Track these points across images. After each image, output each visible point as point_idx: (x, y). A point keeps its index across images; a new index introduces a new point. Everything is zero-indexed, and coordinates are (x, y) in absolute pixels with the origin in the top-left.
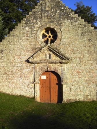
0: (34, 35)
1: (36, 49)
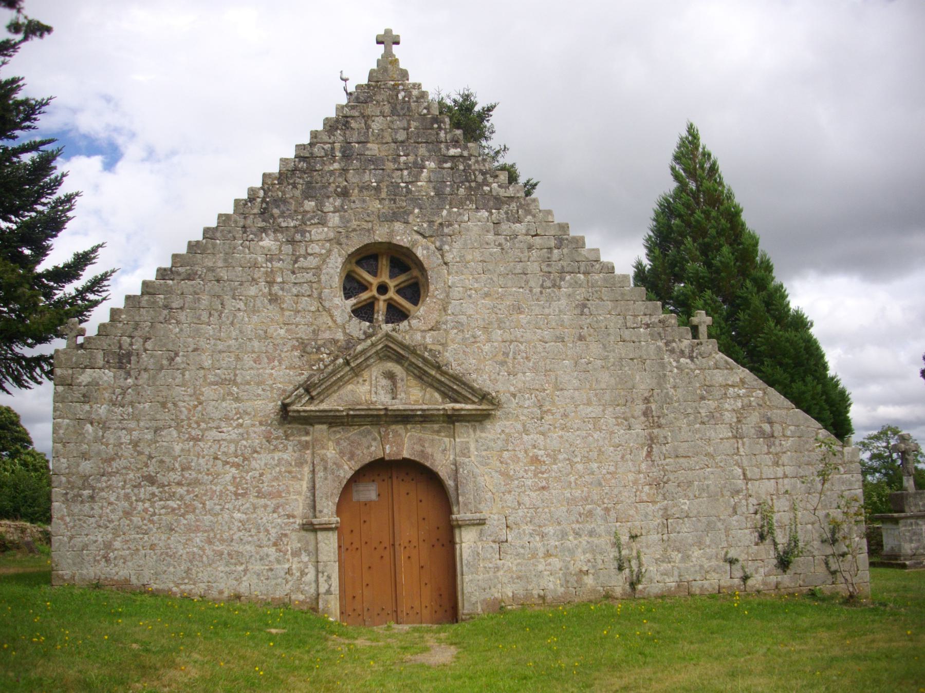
0: (309, 276)
1: (318, 349)
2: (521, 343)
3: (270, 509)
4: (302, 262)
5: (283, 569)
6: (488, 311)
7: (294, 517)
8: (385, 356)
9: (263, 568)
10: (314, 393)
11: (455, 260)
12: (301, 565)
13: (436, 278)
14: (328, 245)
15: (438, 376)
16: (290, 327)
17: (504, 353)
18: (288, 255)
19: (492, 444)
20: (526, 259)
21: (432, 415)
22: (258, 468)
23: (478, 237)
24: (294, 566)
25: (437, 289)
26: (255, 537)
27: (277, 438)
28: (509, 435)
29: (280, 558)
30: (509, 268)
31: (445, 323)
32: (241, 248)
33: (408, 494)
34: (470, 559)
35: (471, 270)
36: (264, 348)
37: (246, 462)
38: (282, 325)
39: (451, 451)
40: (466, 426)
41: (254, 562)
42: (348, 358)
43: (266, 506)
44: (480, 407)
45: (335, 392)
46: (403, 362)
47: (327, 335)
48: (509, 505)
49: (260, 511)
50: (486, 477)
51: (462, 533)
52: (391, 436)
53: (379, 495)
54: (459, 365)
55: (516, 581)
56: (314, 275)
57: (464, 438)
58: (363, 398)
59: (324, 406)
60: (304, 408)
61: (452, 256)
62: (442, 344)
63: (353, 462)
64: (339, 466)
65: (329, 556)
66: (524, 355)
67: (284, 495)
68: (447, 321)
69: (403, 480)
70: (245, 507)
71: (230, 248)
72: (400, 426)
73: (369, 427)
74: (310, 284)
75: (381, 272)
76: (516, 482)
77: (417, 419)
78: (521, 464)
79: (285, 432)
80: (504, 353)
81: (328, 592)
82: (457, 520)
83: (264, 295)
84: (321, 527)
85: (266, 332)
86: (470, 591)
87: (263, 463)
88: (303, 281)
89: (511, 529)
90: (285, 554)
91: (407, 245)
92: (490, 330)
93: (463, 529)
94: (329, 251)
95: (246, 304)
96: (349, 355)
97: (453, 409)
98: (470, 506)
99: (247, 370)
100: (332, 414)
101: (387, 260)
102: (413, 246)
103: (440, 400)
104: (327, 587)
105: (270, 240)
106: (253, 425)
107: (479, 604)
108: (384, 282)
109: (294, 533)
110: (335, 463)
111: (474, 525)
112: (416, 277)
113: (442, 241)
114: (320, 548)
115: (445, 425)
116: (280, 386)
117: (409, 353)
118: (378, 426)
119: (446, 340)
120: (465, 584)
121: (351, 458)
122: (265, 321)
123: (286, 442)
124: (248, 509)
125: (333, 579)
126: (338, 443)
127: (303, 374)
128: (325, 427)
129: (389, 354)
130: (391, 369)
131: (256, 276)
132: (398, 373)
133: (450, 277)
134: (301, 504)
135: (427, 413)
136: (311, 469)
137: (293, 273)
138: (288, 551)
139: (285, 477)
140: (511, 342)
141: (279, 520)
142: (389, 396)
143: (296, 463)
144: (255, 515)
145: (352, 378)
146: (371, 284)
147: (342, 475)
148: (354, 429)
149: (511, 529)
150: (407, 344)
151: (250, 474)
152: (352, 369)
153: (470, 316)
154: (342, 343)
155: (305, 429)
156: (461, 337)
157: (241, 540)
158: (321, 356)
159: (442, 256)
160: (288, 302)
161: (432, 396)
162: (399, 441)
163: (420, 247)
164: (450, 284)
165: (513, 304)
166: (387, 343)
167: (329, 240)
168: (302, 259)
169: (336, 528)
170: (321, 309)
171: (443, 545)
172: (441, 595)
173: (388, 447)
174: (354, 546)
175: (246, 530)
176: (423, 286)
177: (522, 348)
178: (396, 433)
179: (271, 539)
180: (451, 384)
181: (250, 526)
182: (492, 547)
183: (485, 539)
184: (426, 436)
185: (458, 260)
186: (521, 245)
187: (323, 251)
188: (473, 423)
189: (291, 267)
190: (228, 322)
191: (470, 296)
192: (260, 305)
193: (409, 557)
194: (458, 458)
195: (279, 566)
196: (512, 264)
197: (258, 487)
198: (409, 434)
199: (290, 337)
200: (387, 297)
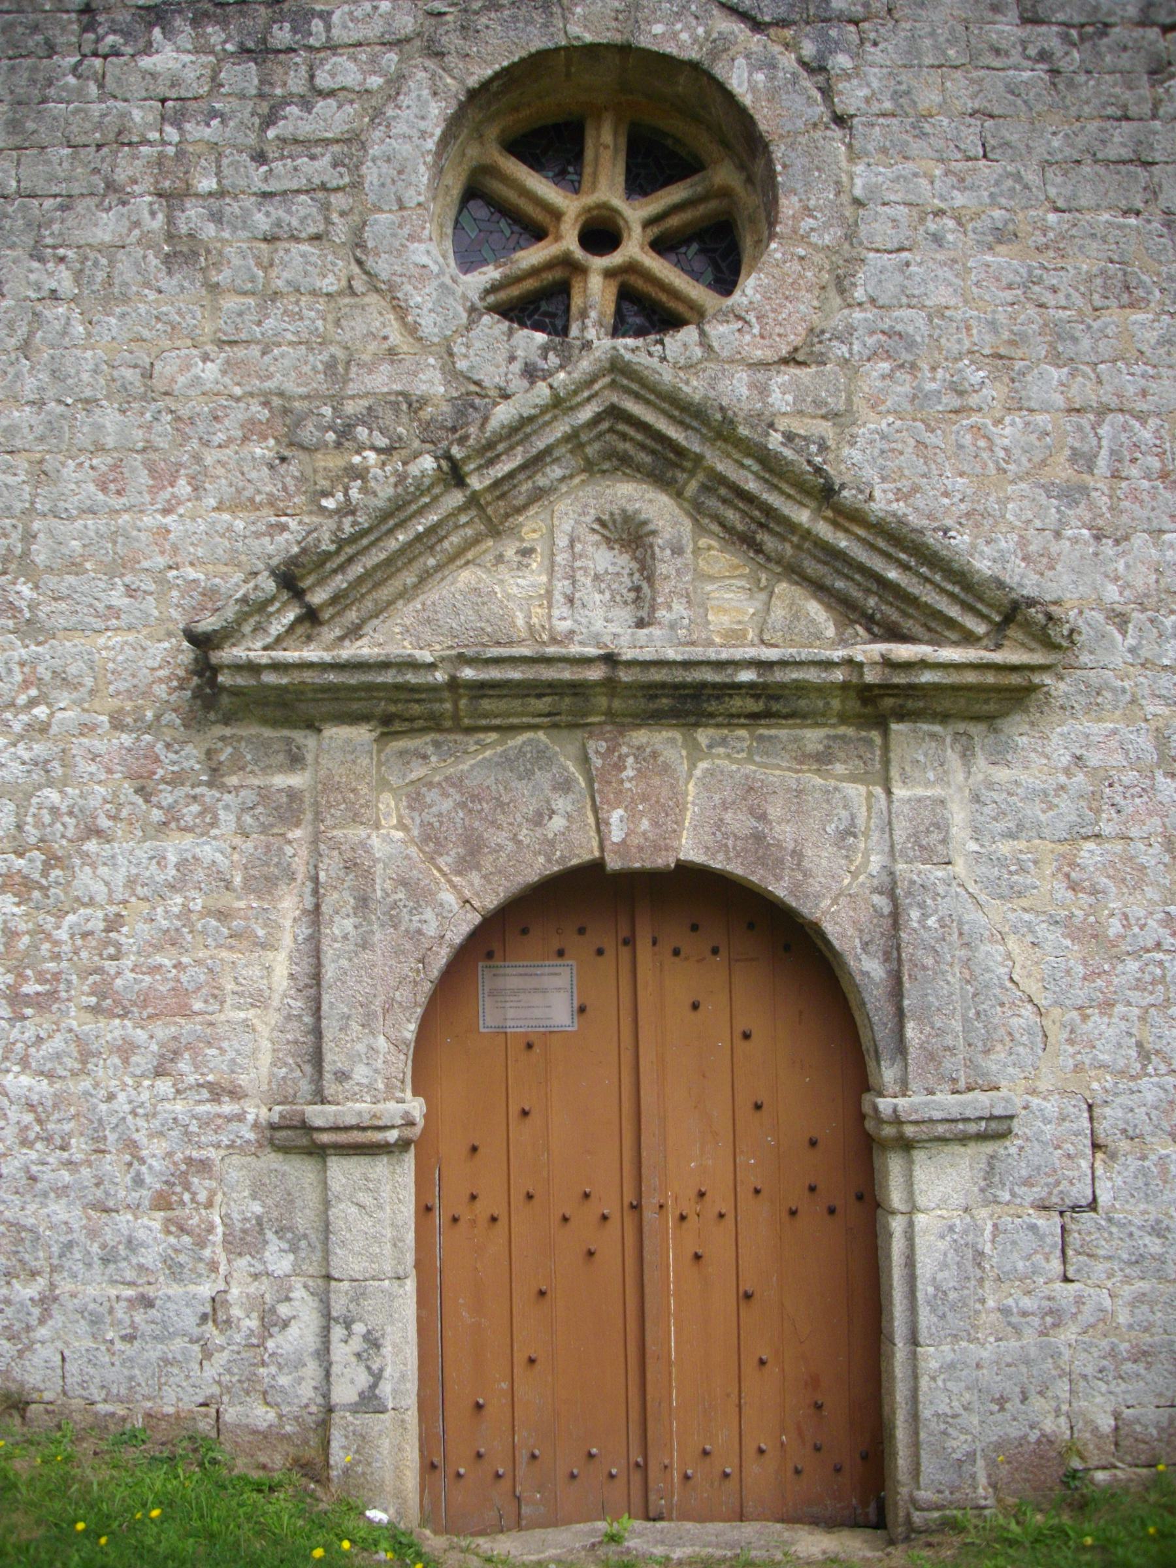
0: (319, 168)
1: (345, 433)
2: (1142, 417)
3: (142, 1062)
4: (294, 122)
5: (192, 1299)
6: (1009, 296)
7: (236, 1094)
8: (609, 454)
9: (113, 1292)
10: (317, 598)
11: (875, 107)
12: (264, 1285)
13: (807, 171)
14: (391, 57)
15: (824, 530)
16: (240, 352)
17: (1075, 455)
18: (242, 96)
19: (1035, 811)
20: (1147, 109)
21: (801, 688)
22: (101, 898)
23: (960, 28)
24: (235, 1291)
25: (808, 211)
26: (85, 1172)
27: (176, 780)
28: (1104, 777)
29: (182, 1258)
30: (1081, 141)
31: (845, 335)
32: (71, 80)
33: (695, 1006)
34: (948, 1278)
35: (941, 144)
36: (139, 434)
37: (56, 873)
38: (209, 348)
39: (875, 836)
40: (933, 736)
41: (79, 1267)
42: (456, 451)
43: (126, 1050)
44: (998, 657)
45: (405, 594)
46: (681, 476)
47: (382, 380)
48: (1105, 1057)
49: (105, 1070)
50: (1012, 943)
51: (919, 1174)
52: (630, 773)
53: (582, 1010)
54: (900, 495)
55: (1129, 1367)
56: (335, 165)
57: (928, 784)
58: (520, 622)
59: (363, 649)
60: (279, 655)
61: (864, 92)
62: (832, 416)
63: (475, 877)
64: (419, 894)
65: (373, 1258)
66: (1156, 464)
67: (198, 1006)
68: (851, 329)
69: (676, 952)
70: (47, 1048)
71: (33, 81)
72: (666, 734)
73: (541, 735)
74: (320, 195)
75: (595, 175)
76: (1133, 966)
77: (737, 703)
78: (1150, 892)
79: (209, 753)
80: (1075, 455)
81: (369, 1402)
82: (897, 1121)
83: (145, 241)
84: (342, 1138)
85: (148, 375)
86: (943, 1408)
87: (120, 878)
88: (295, 186)
89: (1113, 1156)
90: (201, 1244)
91: (693, 54)
92: (1018, 365)
93: (919, 1155)
94: (396, 83)
95: (78, 276)
96: (462, 441)
97: (889, 663)
98: (948, 1064)
99: (70, 518)
100: (388, 677)
101: (615, 134)
102: (715, 55)
103: (831, 632)
104: (363, 1380)
105: (178, 50)
106: (87, 729)
107: (980, 1463)
108: (604, 206)
109: (236, 1160)
110: (403, 883)
111: (964, 1139)
112: (725, 193)
113: (823, 38)
114: (337, 1224)
115: (849, 731)
116: (192, 573)
117: (704, 439)
118: (579, 734)
119: (849, 401)
120: (924, 1382)
121: (464, 865)
122: (146, 333)
123: (209, 794)
124: (58, 1056)
125: (387, 1350)
126: (416, 802)
127: (284, 528)
128: (362, 734)
129: (623, 446)
130: (630, 509)
131: (121, 176)
132: (658, 523)
133: (859, 168)
134: (266, 1045)
135: (779, 676)
136: (309, 902)
137: (260, 158)
138: (211, 1229)
139: (204, 933)
140: (1103, 411)
141: (179, 1107)
142: (625, 615)
143: (246, 880)
144: (86, 1084)
145: (476, 541)
146: (557, 215)
147: (431, 930)
148: (485, 746)
149: (1113, 1156)
150: (697, 398)
151: (71, 918)
152: (474, 500)
153: (941, 311)
154: (440, 409)
155: (289, 741)
156: (907, 389)
157: (33, 1179)
158: (357, 459)
159: (827, 92)
160: (236, 261)
161: (796, 615)
162: (665, 792)
163: (741, 61)
164: (858, 192)
165: (1103, 272)
166: (614, 398)
167: (399, 42)
168: (293, 110)
169: (403, 1145)
170: (359, 286)
171: (832, 1211)
172: (819, 1407)
173: (616, 815)
174: (483, 1208)
175: (48, 1140)
176: (752, 220)
177: (1146, 435)
178: (649, 759)
179: (148, 1180)
180: (877, 564)
181: (67, 1127)
182: (1033, 1228)
183: (1006, 1197)
184: (774, 776)
185: (888, 105)
186: (1125, 60)
187: (375, 81)
188: (961, 727)
189: (252, 139)
190: (12, 342)
191: (937, 239)
192: (130, 275)
193: (697, 1257)
194: (901, 867)
195: (175, 1290)
196: (1092, 127)
197: (99, 970)
198: (703, 765)
199: (238, 391)
200: (616, 259)
